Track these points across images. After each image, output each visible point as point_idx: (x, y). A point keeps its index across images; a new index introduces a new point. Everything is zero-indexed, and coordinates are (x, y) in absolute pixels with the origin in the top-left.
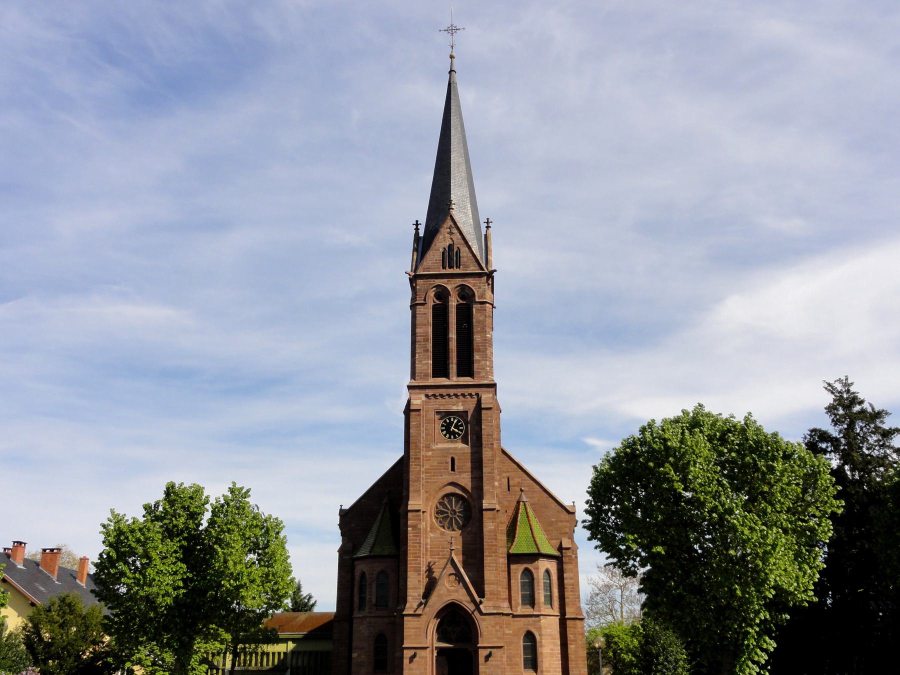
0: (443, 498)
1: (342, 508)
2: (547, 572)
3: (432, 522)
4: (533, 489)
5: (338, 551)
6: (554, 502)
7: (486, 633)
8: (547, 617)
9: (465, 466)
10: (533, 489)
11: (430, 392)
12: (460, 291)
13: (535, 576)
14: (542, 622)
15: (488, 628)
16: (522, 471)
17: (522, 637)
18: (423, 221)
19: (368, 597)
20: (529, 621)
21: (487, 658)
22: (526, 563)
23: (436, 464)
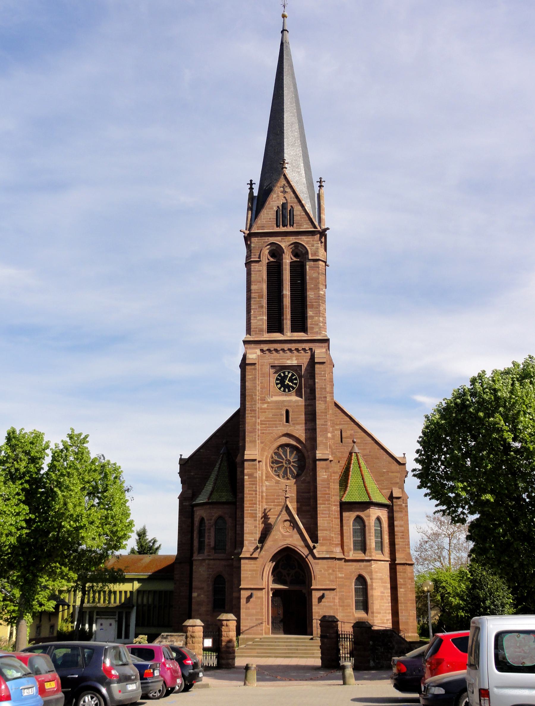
0: (278, 448)
1: (182, 457)
2: (378, 519)
4: (364, 440)
5: (178, 498)
6: (385, 453)
7: (319, 576)
8: (378, 562)
9: (299, 418)
10: (364, 440)
11: (265, 347)
12: (294, 248)
13: (367, 524)
14: (373, 566)
15: (321, 571)
17: (354, 581)
18: (257, 181)
19: (206, 541)
23: (271, 416)
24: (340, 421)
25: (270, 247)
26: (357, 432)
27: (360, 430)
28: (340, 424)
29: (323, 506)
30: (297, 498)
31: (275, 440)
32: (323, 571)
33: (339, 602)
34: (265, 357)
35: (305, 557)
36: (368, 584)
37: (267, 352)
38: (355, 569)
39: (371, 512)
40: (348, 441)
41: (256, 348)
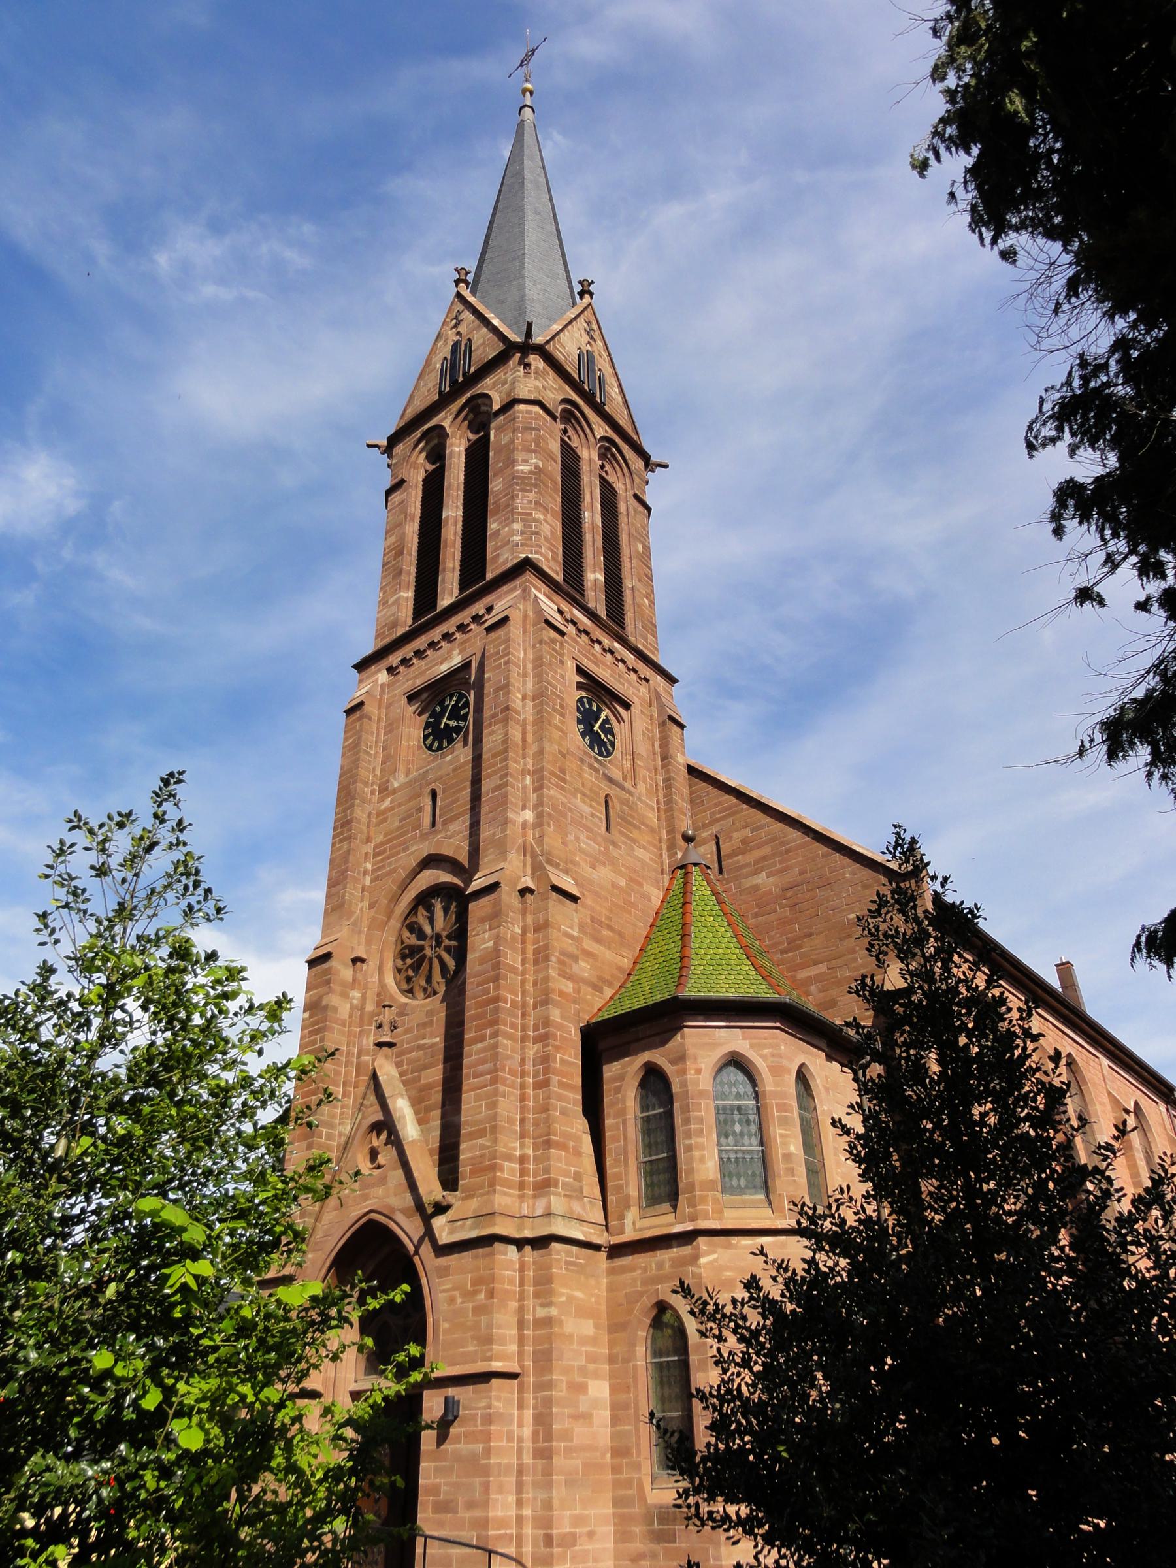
0: (413, 910)
3: (382, 985)
4: (783, 844)
6: (847, 861)
7: (446, 1325)
8: (734, 1240)
9: (457, 800)
10: (783, 844)
11: (394, 659)
12: (471, 416)
13: (676, 1088)
14: (703, 1260)
15: (452, 1300)
16: (753, 807)
17: (642, 1334)
20: (660, 1266)
21: (444, 1426)
22: (644, 1049)
23: (397, 824)
24: (712, 814)
25: (427, 444)
26: (761, 827)
27: (766, 820)
28: (711, 824)
29: (479, 1046)
30: (445, 1047)
31: (404, 887)
32: (459, 1300)
33: (535, 1434)
34: (398, 681)
35: (411, 1249)
36: (690, 1342)
37: (401, 669)
38: (645, 1283)
39: (689, 1042)
40: (738, 862)
41: (379, 671)
